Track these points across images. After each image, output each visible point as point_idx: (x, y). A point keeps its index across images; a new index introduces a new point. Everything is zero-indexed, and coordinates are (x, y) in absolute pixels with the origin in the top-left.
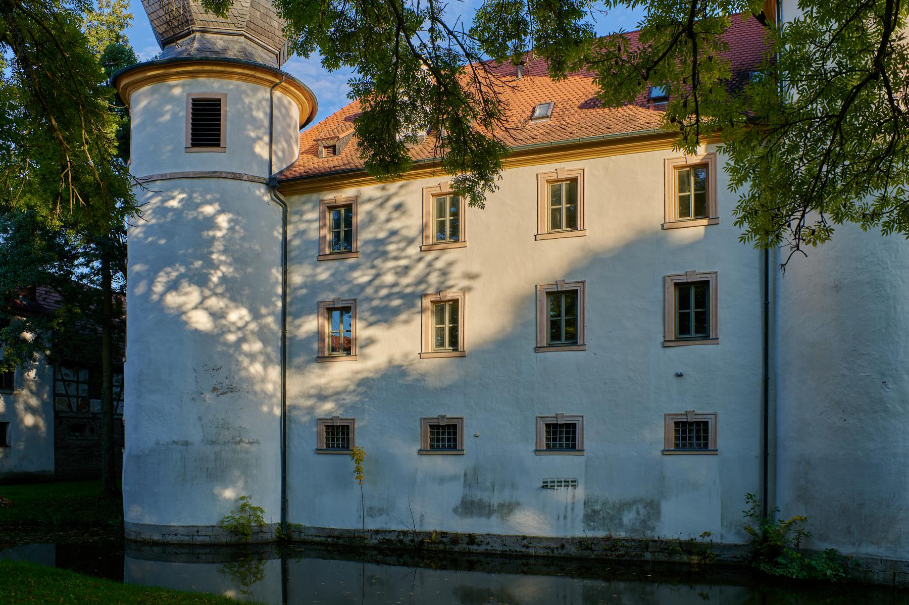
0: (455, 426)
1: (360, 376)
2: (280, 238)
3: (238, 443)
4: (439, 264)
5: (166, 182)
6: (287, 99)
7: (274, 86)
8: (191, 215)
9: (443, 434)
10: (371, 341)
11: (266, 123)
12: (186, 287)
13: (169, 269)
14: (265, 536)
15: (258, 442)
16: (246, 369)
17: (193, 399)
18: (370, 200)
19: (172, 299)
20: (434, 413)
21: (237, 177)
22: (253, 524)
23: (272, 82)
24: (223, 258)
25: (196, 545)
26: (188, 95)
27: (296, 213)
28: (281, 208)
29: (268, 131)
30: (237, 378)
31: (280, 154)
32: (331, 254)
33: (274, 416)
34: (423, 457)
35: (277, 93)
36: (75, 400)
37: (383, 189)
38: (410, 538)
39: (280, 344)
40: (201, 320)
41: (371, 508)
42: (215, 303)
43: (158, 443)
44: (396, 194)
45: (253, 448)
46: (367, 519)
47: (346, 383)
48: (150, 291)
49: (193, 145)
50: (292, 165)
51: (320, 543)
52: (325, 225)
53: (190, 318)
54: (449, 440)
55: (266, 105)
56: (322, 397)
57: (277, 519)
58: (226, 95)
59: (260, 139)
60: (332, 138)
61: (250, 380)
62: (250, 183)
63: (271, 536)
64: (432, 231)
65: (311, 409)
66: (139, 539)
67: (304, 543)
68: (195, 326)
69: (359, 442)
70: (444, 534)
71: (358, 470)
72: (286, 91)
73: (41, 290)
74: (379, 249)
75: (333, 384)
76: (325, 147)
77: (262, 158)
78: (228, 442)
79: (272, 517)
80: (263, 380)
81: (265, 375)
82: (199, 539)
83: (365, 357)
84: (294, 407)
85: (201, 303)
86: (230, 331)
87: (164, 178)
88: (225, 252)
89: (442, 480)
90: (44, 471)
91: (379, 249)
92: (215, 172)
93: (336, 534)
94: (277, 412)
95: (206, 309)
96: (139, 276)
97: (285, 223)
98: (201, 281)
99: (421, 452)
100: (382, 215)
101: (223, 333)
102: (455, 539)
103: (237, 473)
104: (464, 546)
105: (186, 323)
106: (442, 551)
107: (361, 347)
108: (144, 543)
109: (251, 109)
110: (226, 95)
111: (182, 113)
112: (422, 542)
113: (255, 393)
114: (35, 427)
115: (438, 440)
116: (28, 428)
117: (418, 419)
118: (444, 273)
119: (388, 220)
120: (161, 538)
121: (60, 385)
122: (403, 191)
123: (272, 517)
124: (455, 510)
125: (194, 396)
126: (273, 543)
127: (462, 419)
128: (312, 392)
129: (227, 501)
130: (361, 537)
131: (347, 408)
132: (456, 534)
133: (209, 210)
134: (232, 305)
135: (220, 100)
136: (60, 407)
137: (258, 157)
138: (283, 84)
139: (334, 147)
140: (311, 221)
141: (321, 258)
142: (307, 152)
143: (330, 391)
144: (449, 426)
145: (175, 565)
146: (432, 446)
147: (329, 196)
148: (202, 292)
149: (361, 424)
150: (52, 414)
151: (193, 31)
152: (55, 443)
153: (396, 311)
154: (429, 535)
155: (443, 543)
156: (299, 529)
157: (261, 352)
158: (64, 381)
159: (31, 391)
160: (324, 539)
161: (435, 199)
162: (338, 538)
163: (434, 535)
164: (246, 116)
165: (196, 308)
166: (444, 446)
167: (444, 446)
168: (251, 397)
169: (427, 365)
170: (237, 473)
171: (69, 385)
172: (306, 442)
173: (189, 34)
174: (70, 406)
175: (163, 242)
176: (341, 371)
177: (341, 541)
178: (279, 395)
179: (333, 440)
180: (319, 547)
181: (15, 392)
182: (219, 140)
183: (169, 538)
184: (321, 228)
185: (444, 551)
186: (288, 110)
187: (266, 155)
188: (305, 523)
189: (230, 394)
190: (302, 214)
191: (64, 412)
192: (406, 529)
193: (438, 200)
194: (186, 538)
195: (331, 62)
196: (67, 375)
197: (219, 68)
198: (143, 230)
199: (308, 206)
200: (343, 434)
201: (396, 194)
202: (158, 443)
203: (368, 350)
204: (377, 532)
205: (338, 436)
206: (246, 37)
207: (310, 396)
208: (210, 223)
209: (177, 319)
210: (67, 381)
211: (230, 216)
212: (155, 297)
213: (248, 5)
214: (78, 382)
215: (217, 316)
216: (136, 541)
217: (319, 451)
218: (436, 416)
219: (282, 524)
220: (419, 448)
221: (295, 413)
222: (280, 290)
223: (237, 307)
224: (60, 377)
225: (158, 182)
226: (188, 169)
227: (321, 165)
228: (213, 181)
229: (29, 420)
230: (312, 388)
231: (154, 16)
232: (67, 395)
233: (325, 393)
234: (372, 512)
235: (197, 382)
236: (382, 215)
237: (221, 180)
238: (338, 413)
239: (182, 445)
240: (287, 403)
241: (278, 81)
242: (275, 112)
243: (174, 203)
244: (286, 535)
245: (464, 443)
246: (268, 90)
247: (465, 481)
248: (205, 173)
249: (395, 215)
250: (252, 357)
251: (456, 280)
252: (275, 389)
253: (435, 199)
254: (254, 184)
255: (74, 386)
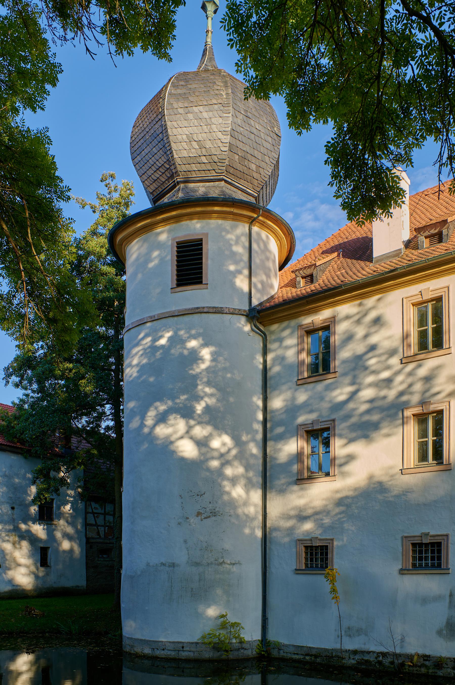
0: (439, 544)
1: (339, 496)
2: (261, 367)
3: (221, 564)
4: (423, 372)
5: (155, 322)
6: (264, 234)
7: (252, 221)
8: (175, 352)
9: (426, 551)
10: (350, 458)
11: (246, 258)
12: (172, 419)
13: (158, 404)
14: (245, 652)
15: (239, 563)
16: (229, 493)
17: (179, 524)
18: (347, 317)
19: (162, 431)
20: (417, 530)
21: (218, 311)
22: (234, 641)
23: (250, 217)
24: (207, 390)
25: (181, 660)
26: (173, 239)
27: (275, 341)
28: (261, 338)
29: (248, 264)
30: (220, 502)
31: (259, 286)
32: (309, 377)
33: (256, 537)
34: (404, 576)
35: (255, 229)
36: (102, 529)
37: (360, 305)
38: (389, 660)
39: (260, 468)
40: (187, 449)
41: (349, 628)
42: (199, 431)
43: (148, 565)
44: (373, 308)
45: (235, 569)
46: (345, 639)
47: (324, 502)
48: (142, 425)
49: (178, 285)
50: (272, 297)
51: (299, 661)
52: (303, 349)
53: (177, 447)
54: (433, 559)
55: (244, 240)
56: (302, 518)
57: (257, 636)
58: (207, 235)
59: (239, 272)
60: (310, 267)
61: (232, 503)
62: (231, 316)
63: (251, 653)
64: (414, 339)
65: (291, 530)
66: (132, 652)
67: (283, 660)
68: (181, 454)
69: (339, 563)
70: (426, 657)
71: (334, 590)
72: (263, 225)
73: (74, 440)
74: (358, 364)
75: (312, 505)
76: (303, 278)
77: (242, 290)
78: (212, 563)
79: (251, 633)
80: (246, 503)
81: (244, 496)
82: (184, 655)
83: (344, 475)
84: (276, 529)
85: (187, 432)
86: (213, 458)
87: (153, 319)
88: (208, 384)
89: (425, 600)
90: (78, 586)
91: (358, 364)
92: (198, 308)
93: (314, 652)
94: (259, 533)
95: (191, 438)
96: (133, 413)
97: (265, 352)
98: (187, 413)
99: (402, 572)
100: (360, 332)
101: (207, 460)
102: (439, 663)
103: (219, 591)
104: (449, 670)
105: (174, 452)
106: (424, 675)
107: (341, 465)
108: (137, 656)
109: (231, 245)
110: (207, 235)
111: (169, 257)
112: (403, 665)
113: (238, 516)
114: (71, 551)
115: (421, 559)
116: (64, 551)
117: (399, 537)
118: (428, 379)
119: (366, 336)
120: (150, 652)
121: (90, 517)
122: (381, 304)
123: (251, 633)
124: (439, 633)
125: (180, 520)
126: (254, 658)
127: (447, 536)
128: (292, 513)
129: (209, 619)
130: (339, 657)
131: (326, 529)
132: (440, 657)
133: (193, 344)
134: (215, 433)
135: (201, 240)
136: (90, 535)
137: (239, 291)
138: (260, 218)
139: (311, 276)
140: (290, 347)
141: (300, 382)
142: (286, 286)
143: (310, 512)
144: (433, 544)
145: (163, 677)
146: (414, 565)
147: (307, 320)
148: (187, 423)
149: (340, 543)
150: (84, 540)
151: (178, 183)
152: (87, 564)
153: (376, 426)
154: (410, 657)
155: (426, 666)
156: (279, 647)
157: (243, 476)
158: (93, 513)
159: (67, 522)
160: (302, 657)
161: (416, 308)
162: (316, 656)
163: (416, 658)
164: (227, 253)
165: (182, 438)
166: (427, 565)
167: (427, 565)
168: (233, 520)
169: (408, 480)
170: (219, 591)
171: (97, 517)
172: (286, 562)
173: (174, 186)
174: (98, 533)
175: (152, 379)
176: (320, 492)
177: (318, 660)
178: (260, 518)
179: (311, 560)
180: (297, 665)
181: (54, 523)
182: (201, 278)
183: (158, 653)
184: (300, 352)
185: (426, 675)
186: (266, 245)
187: (246, 289)
188: (284, 640)
189: (214, 518)
190: (281, 340)
191: (93, 538)
192: (385, 651)
193: (419, 310)
194: (173, 653)
195: (299, 119)
196: (96, 508)
197: (199, 209)
198: (137, 369)
199: (287, 333)
200: (322, 554)
201: (373, 308)
202: (148, 565)
203: (347, 468)
204: (355, 652)
205: (317, 556)
206: (226, 181)
207: (289, 517)
208: (194, 357)
209: (166, 449)
210: (96, 513)
211: (212, 349)
212: (146, 430)
213: (226, 149)
214: (105, 514)
215: (202, 444)
216: (130, 654)
217: (298, 571)
218: (418, 534)
219: (262, 641)
220: (400, 567)
221: (274, 534)
222: (260, 416)
223: (220, 436)
224: (90, 511)
225: (148, 324)
226: (174, 309)
227: (299, 293)
228: (196, 316)
229: (66, 545)
230: (293, 509)
231: (145, 177)
232: (96, 525)
233: (304, 514)
234: (350, 632)
235: (183, 508)
236: (360, 332)
237: (203, 315)
238: (318, 533)
239: (169, 566)
240: (268, 525)
241: (255, 216)
242: (254, 246)
243: (163, 341)
244: (266, 651)
245: (450, 561)
246: (247, 226)
247: (450, 602)
248: (189, 309)
249: (373, 330)
250: (234, 481)
251: (442, 385)
252: (257, 512)
253: (416, 308)
254: (235, 316)
255: (102, 517)
